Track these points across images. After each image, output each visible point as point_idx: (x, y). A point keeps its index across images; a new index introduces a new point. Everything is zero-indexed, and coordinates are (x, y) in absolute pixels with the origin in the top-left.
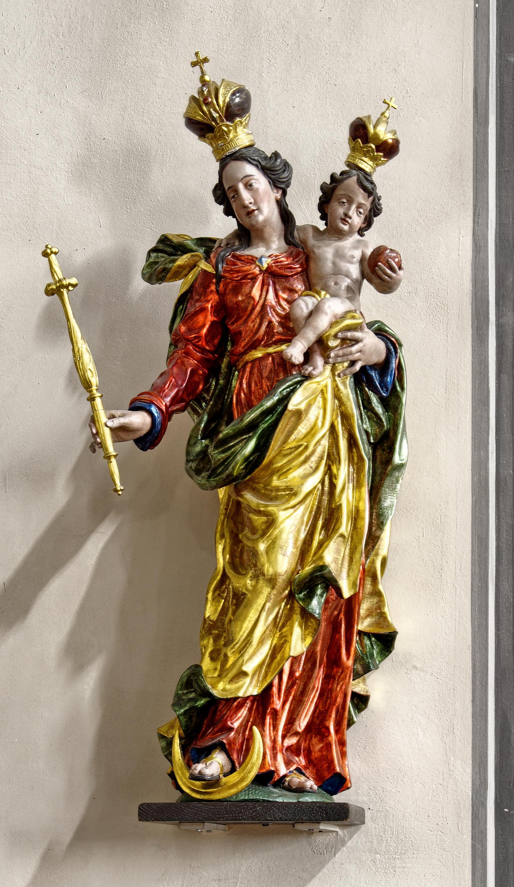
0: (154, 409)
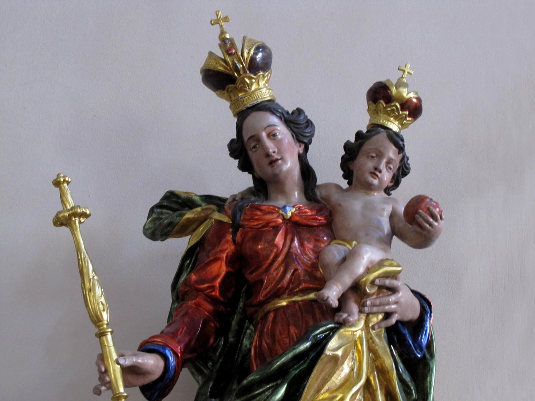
0: (168, 353)
